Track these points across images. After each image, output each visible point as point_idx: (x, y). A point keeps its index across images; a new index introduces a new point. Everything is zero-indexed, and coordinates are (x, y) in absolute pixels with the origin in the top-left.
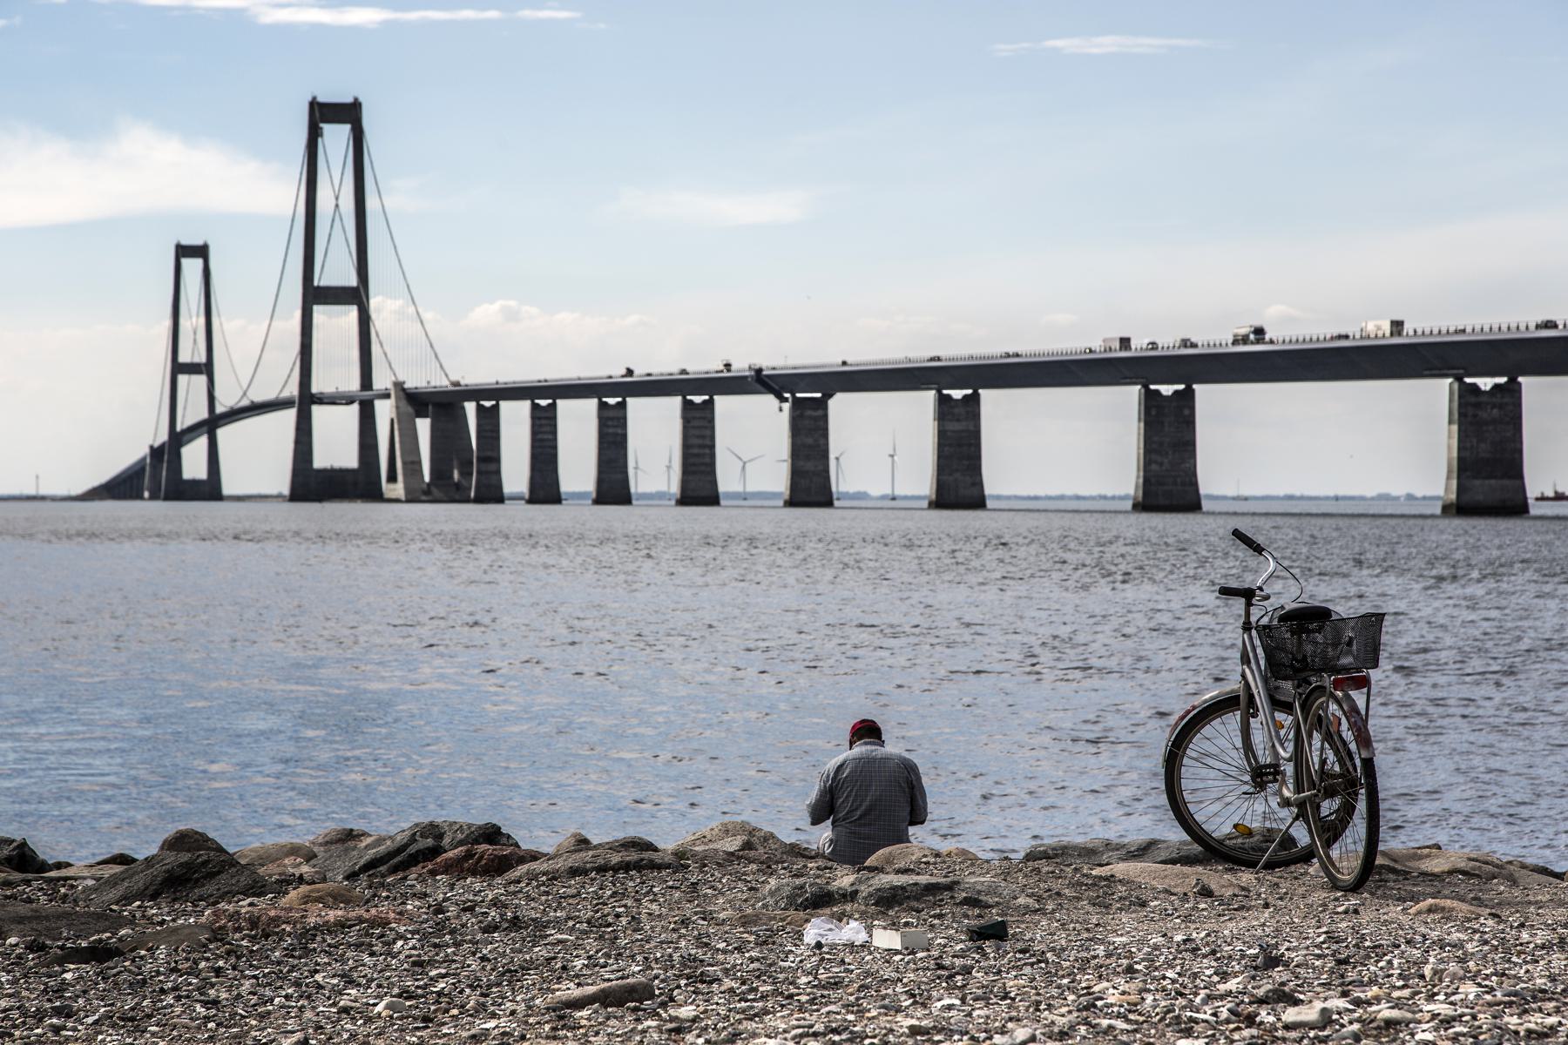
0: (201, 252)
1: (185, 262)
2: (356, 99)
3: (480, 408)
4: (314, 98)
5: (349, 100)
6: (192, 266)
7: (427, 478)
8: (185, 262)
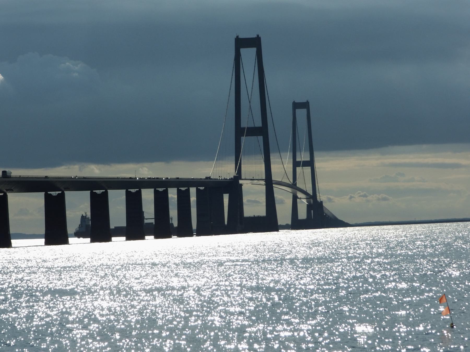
0: (305, 105)
1: (243, 51)
2: (258, 36)
3: (179, 192)
4: (237, 37)
5: (255, 36)
6: (302, 113)
7: (226, 223)
8: (298, 111)
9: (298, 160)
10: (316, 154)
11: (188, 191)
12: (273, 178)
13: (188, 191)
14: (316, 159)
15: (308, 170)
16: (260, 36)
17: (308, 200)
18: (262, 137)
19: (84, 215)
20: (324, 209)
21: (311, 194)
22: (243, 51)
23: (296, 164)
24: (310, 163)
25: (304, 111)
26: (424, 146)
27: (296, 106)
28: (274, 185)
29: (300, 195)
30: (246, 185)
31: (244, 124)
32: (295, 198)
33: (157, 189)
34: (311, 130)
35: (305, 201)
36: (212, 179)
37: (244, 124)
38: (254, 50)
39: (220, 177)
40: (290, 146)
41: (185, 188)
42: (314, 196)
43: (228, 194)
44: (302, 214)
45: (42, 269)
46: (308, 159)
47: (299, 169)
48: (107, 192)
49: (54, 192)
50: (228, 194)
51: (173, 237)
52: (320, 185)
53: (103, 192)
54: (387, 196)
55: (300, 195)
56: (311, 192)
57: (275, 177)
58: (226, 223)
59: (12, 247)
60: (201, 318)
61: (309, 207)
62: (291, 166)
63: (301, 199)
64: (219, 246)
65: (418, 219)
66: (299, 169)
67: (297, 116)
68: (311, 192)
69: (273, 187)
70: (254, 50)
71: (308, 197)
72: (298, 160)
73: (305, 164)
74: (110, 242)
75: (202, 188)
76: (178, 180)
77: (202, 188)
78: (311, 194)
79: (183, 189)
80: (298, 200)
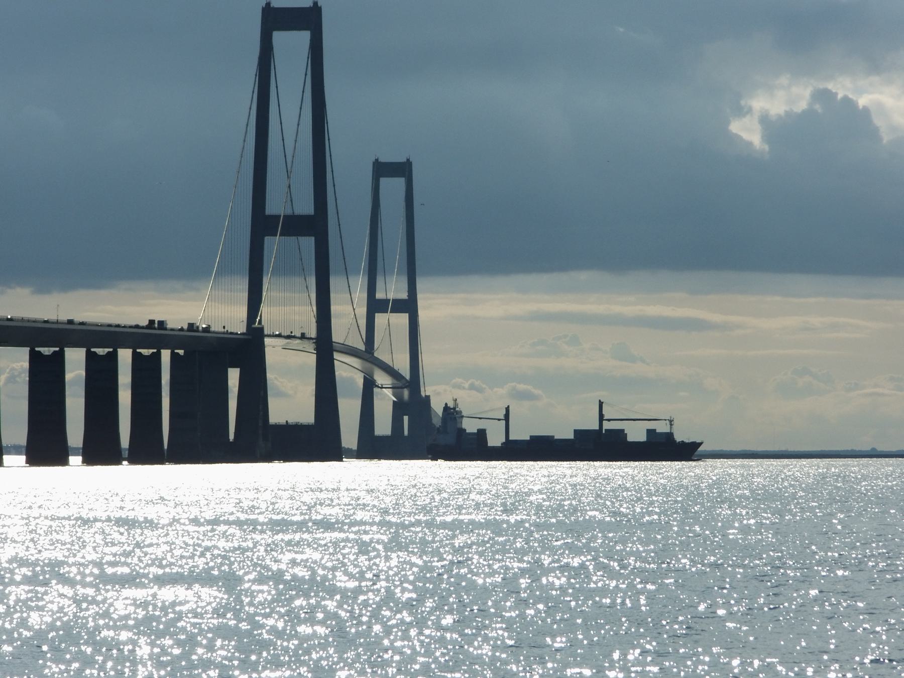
0: (403, 170)
1: (278, 37)
3: (91, 358)
6: (393, 187)
7: (232, 437)
8: (384, 182)
9: (380, 295)
10: (420, 284)
11: (113, 357)
12: (335, 338)
13: (112, 358)
14: (420, 297)
15: (402, 320)
16: (319, 5)
17: (395, 390)
18: (313, 238)
19: (451, 405)
20: (432, 412)
21: (408, 377)
22: (278, 37)
23: (375, 306)
24: (409, 306)
25: (399, 183)
26: (583, 276)
27: (382, 170)
28: (336, 356)
29: (381, 378)
30: (274, 351)
31: (275, 205)
32: (369, 385)
33: (37, 349)
34: (413, 228)
35: (388, 393)
36: (214, 332)
37: (275, 205)
38: (305, 37)
39: (224, 327)
40: (364, 264)
41: (107, 350)
42: (414, 382)
43: (238, 370)
44: (383, 426)
45: (369, 508)
46: (404, 295)
47: (381, 319)
48: (160, 352)
49: (46, 349)
50: (238, 370)
51: (344, 460)
52: (426, 359)
53: (109, 352)
54: (529, 387)
55: (381, 378)
56: (406, 372)
57: (338, 335)
58: (232, 437)
59: (3, 466)
60: (398, 638)
61: (399, 408)
62: (362, 311)
63: (382, 388)
64: (279, 489)
65: (792, 448)
66: (381, 319)
67: (381, 191)
68: (406, 372)
69: (332, 359)
70: (305, 37)
71: (399, 384)
72: (380, 295)
73: (399, 306)
74: (67, 467)
75: (181, 352)
76: (182, 333)
77: (181, 352)
78: (408, 377)
79: (101, 351)
80: (376, 390)
